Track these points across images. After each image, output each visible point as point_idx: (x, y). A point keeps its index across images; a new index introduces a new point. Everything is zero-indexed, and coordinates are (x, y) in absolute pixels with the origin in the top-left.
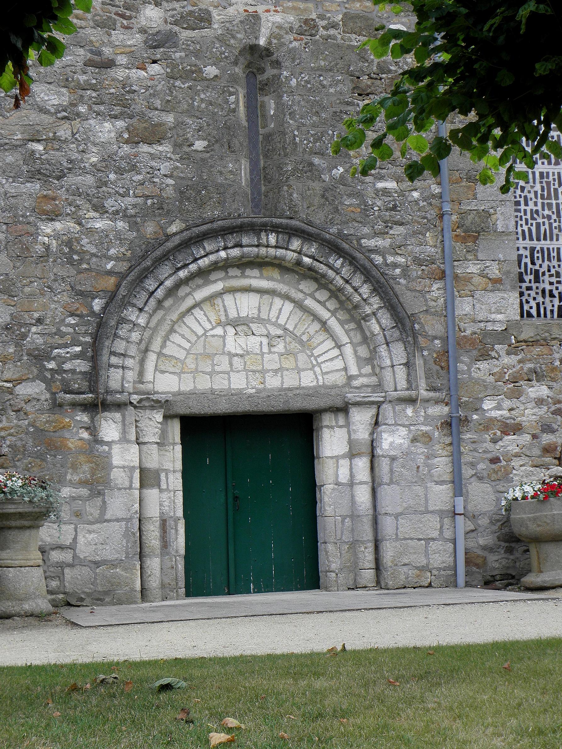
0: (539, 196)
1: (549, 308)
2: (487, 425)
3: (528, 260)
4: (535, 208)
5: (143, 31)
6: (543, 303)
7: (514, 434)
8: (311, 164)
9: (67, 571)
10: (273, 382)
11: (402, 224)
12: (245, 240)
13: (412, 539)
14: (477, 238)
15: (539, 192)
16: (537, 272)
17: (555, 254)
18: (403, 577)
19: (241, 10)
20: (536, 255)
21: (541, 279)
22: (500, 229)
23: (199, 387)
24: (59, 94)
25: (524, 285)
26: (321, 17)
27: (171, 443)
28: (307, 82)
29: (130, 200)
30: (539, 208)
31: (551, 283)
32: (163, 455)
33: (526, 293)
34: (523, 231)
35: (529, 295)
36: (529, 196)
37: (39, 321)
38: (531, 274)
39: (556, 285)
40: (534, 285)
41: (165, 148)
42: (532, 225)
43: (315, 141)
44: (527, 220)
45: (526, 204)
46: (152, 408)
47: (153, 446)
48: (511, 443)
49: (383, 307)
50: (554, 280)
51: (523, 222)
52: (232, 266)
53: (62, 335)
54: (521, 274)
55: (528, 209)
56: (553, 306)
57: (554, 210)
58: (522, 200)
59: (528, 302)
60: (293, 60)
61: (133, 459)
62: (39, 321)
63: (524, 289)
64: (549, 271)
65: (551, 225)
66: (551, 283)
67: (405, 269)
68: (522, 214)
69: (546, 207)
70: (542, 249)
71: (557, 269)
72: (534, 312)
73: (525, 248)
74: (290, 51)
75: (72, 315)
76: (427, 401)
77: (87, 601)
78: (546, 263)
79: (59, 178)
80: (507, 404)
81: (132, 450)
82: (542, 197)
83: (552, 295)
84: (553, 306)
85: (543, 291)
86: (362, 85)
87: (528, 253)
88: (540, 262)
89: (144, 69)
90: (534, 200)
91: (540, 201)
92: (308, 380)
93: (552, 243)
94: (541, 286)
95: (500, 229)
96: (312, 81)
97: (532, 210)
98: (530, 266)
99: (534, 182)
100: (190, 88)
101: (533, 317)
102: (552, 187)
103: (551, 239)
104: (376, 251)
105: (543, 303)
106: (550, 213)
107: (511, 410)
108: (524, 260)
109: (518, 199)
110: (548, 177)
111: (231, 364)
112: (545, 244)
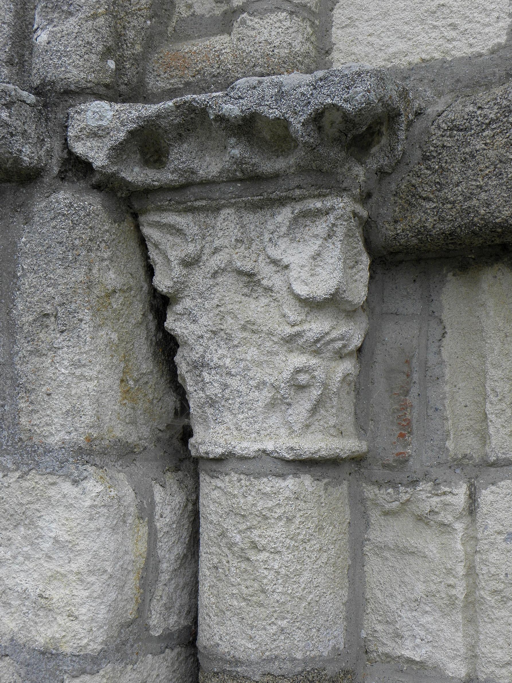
27: (459, 463)
32: (405, 552)
46: (255, 190)
47: (267, 484)
49: (472, 497)
61: (57, 594)
81: (54, 524)
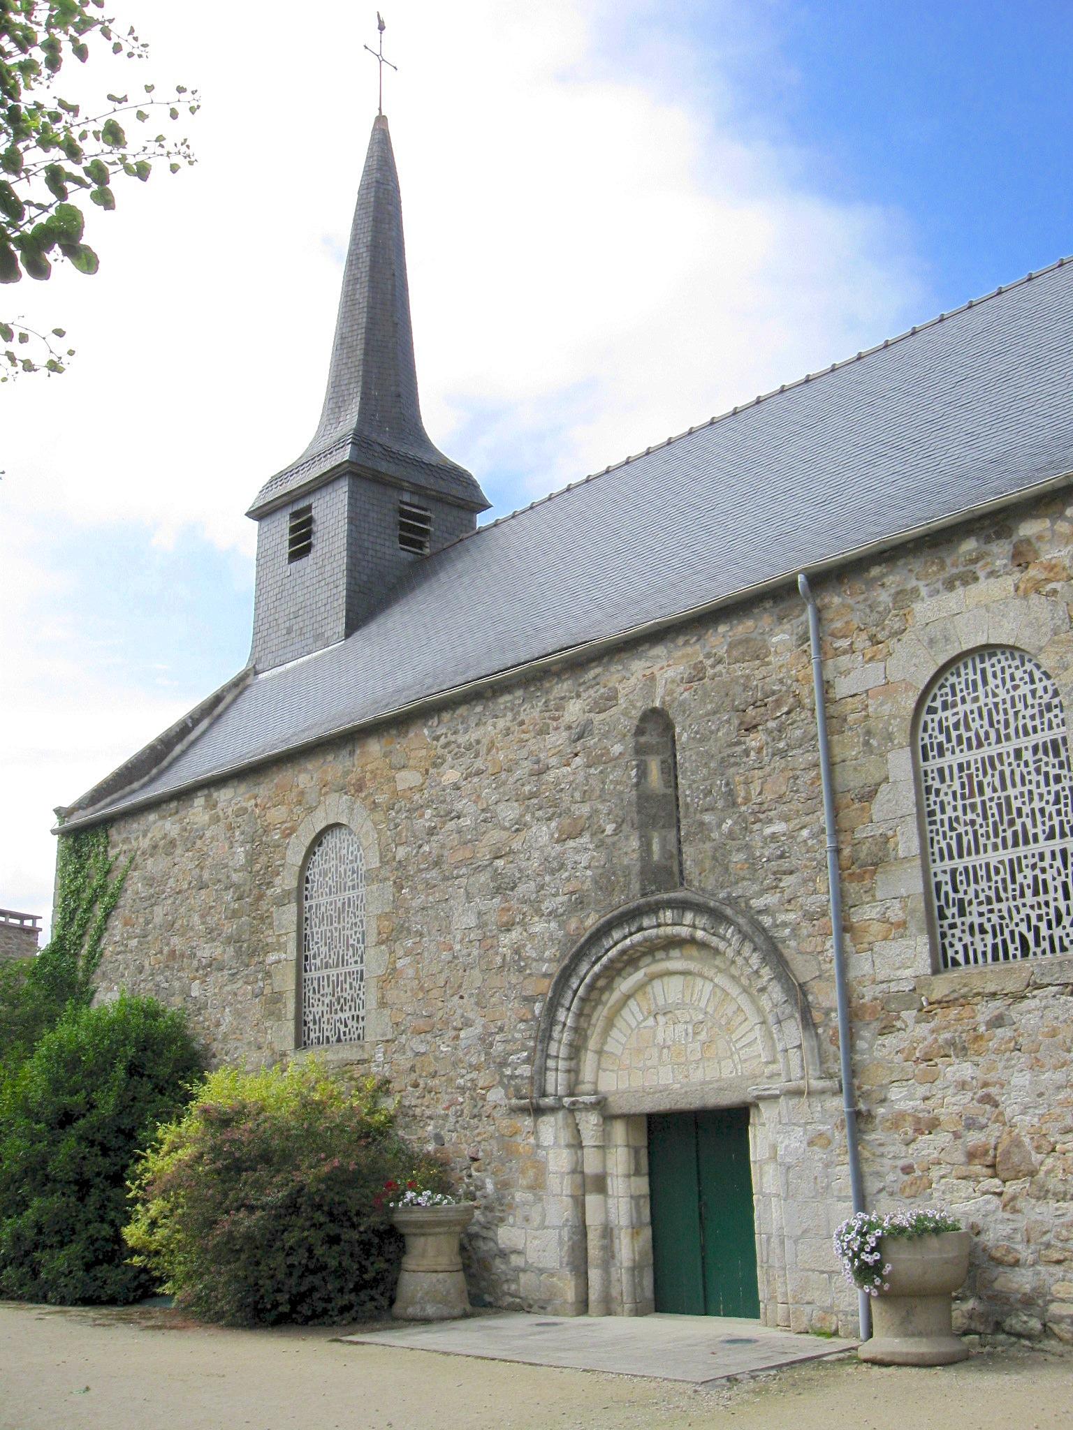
0: (959, 796)
1: (980, 950)
2: (897, 1121)
3: (949, 888)
4: (953, 815)
5: (569, 728)
6: (972, 944)
7: (930, 1133)
8: (702, 824)
9: (521, 1275)
10: (697, 1076)
11: (791, 873)
12: (646, 922)
13: (813, 1270)
14: (874, 872)
15: (959, 792)
16: (961, 901)
17: (984, 873)
18: (805, 1319)
19: (640, 677)
20: (959, 878)
21: (968, 910)
22: (901, 854)
23: (633, 1085)
24: (512, 809)
25: (946, 923)
26: (708, 656)
28: (697, 733)
29: (560, 899)
30: (960, 813)
31: (981, 914)
33: (950, 932)
34: (941, 850)
35: (953, 936)
36: (946, 799)
37: (501, 1029)
38: (954, 905)
39: (987, 915)
40: (958, 921)
41: (585, 839)
42: (951, 838)
43: (705, 796)
44: (944, 833)
45: (943, 811)
48: (928, 1146)
50: (984, 908)
51: (940, 837)
52: (658, 949)
53: (514, 1040)
54: (941, 908)
55: (945, 817)
56: (985, 946)
57: (979, 811)
58: (937, 808)
59: (952, 945)
60: (684, 712)
62: (501, 1029)
63: (946, 928)
64: (977, 897)
65: (975, 832)
66: (981, 914)
67: (795, 928)
68: (938, 826)
69: (968, 810)
70: (966, 869)
71: (987, 892)
72: (960, 958)
73: (945, 872)
74: (682, 704)
75: (522, 1021)
76: (823, 1092)
77: (535, 1308)
78: (973, 886)
79: (512, 889)
80: (922, 1090)
82: (963, 797)
83: (983, 931)
84: (985, 946)
85: (971, 926)
86: (747, 719)
87: (947, 878)
88: (964, 886)
89: (569, 765)
90: (953, 803)
91: (960, 803)
92: (727, 1071)
93: (1029, 847)
94: (968, 920)
95: (901, 854)
96: (702, 731)
97: (950, 818)
98: (951, 895)
99: (952, 780)
100: (601, 772)
101: (959, 964)
102: (975, 780)
103: (977, 852)
104: (765, 911)
105: (972, 944)
106: (974, 817)
107: (926, 1099)
108: (944, 888)
109: (933, 807)
110: (969, 768)
111: (660, 1057)
112: (969, 861)
